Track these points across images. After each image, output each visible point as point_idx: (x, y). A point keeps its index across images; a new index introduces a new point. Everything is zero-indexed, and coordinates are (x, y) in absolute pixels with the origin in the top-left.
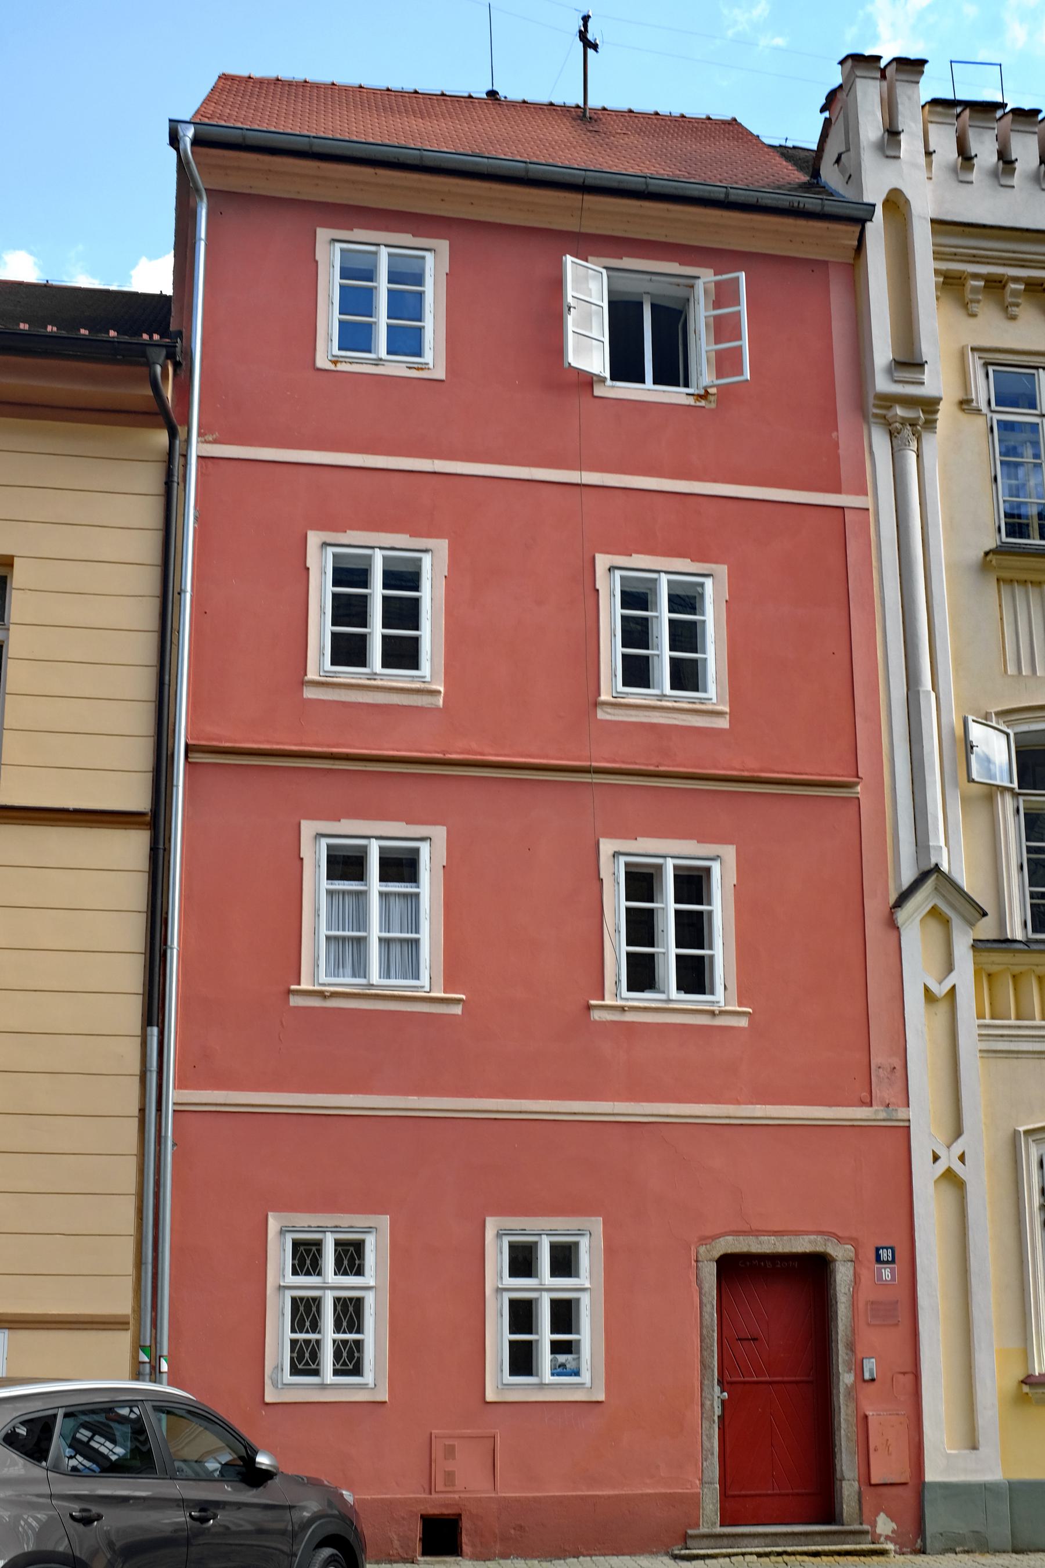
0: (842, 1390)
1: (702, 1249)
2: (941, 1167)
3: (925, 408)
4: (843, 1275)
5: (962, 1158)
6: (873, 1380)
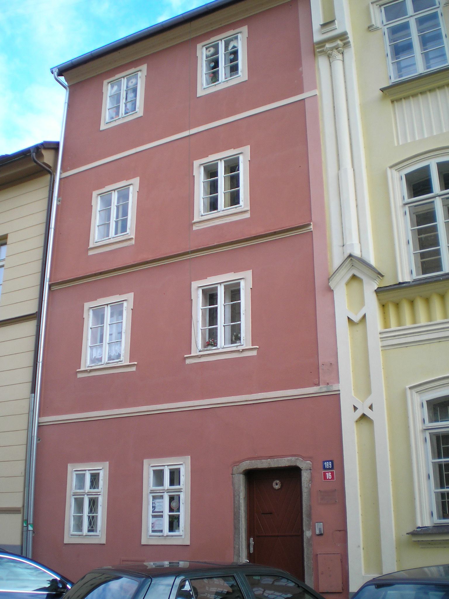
0: (305, 540)
1: (235, 468)
2: (358, 414)
3: (341, 38)
4: (305, 476)
5: (371, 407)
6: (321, 535)
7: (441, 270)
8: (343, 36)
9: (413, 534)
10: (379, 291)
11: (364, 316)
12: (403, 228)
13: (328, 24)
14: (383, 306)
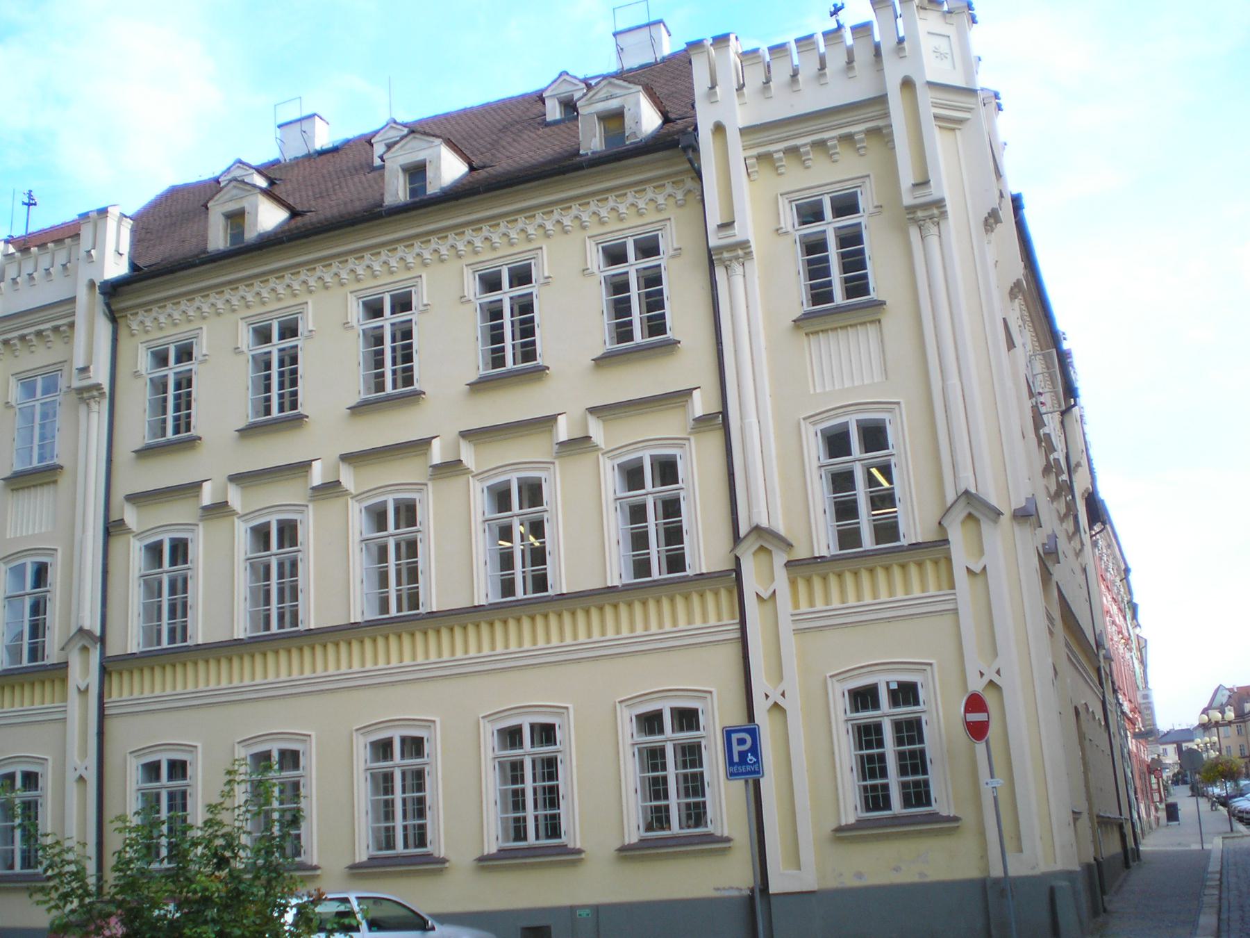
2: (770, 702)
7: (898, 539)
8: (744, 245)
9: (482, 859)
10: (789, 564)
11: (985, 568)
12: (820, 496)
13: (727, 225)
14: (793, 583)
